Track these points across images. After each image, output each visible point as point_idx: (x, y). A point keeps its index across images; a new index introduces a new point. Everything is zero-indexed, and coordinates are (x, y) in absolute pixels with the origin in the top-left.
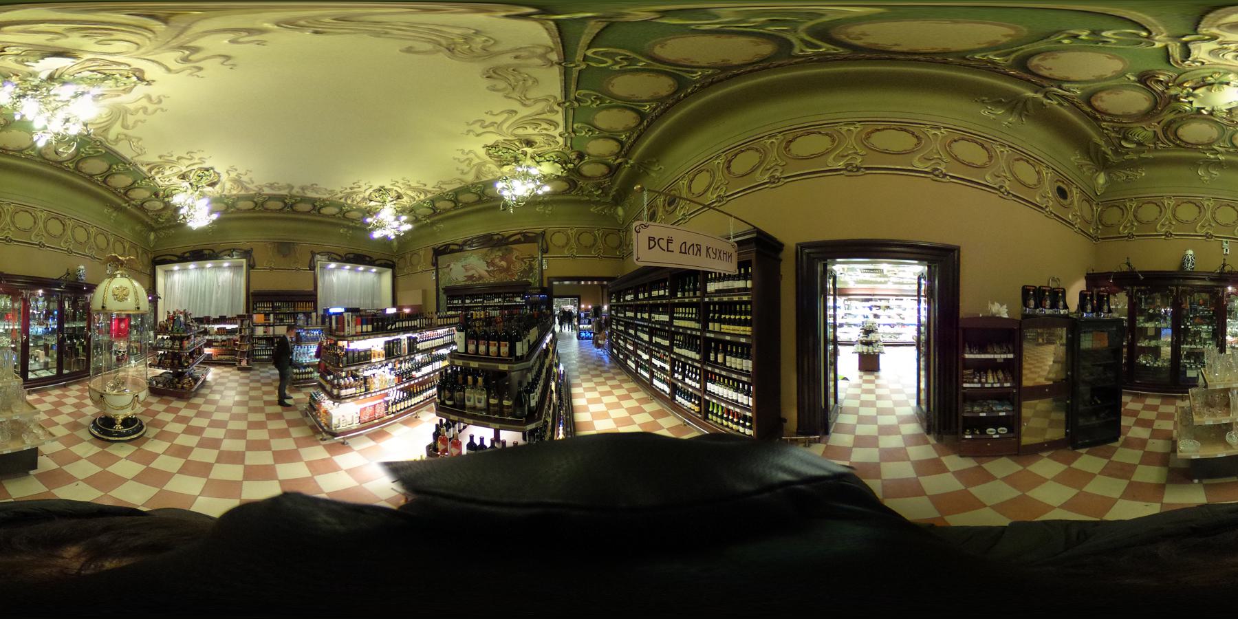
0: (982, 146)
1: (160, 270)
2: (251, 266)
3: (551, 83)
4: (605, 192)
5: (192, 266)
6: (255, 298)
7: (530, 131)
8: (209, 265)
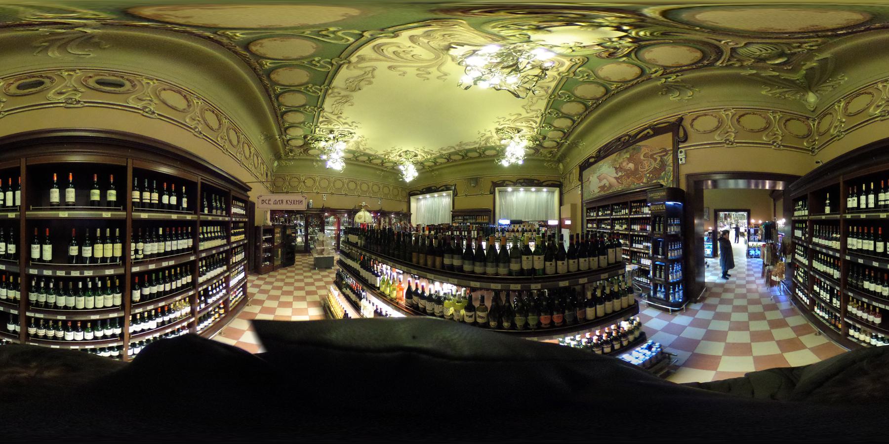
0: (185, 97)
1: (413, 199)
2: (455, 194)
3: (542, 105)
4: (554, 156)
5: (428, 196)
6: (455, 214)
7: (519, 124)
8: (436, 195)
